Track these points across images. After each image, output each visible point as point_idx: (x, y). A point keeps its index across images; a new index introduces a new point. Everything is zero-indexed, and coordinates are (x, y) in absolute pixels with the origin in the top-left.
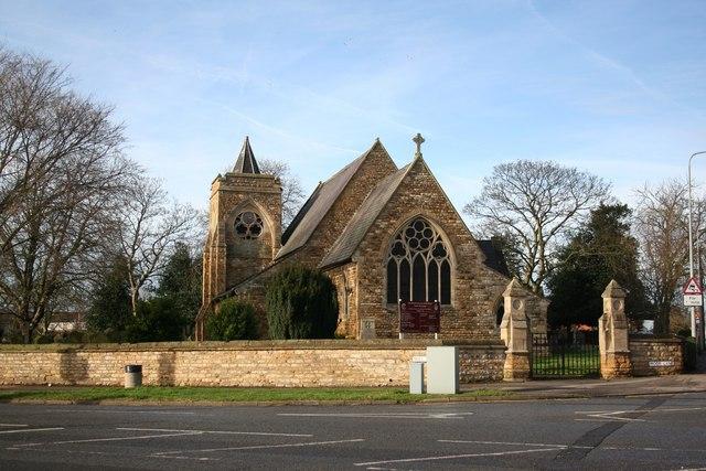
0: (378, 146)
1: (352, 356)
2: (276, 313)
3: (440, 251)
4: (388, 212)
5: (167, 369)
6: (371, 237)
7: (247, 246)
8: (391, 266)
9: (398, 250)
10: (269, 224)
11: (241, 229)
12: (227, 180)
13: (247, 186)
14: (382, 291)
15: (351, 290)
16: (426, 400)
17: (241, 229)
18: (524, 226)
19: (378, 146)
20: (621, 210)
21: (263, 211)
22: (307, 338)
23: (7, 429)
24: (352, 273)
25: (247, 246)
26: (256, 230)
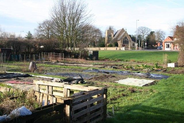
0: (123, 28)
1: (4, 66)
2: (114, 45)
3: (128, 39)
4: (123, 36)
5: (106, 49)
6: (122, 38)
7: (110, 37)
8: (123, 41)
9: (124, 39)
10: (112, 35)
11: (109, 36)
12: (108, 31)
13: (110, 30)
14: (122, 43)
15: (119, 43)
16: (123, 51)
17: (109, 36)
18: (142, 34)
19: (123, 28)
20: (154, 32)
21: (112, 34)
22: (77, 112)
23: (15, 70)
24: (120, 41)
25: (110, 37)
26: (111, 36)
